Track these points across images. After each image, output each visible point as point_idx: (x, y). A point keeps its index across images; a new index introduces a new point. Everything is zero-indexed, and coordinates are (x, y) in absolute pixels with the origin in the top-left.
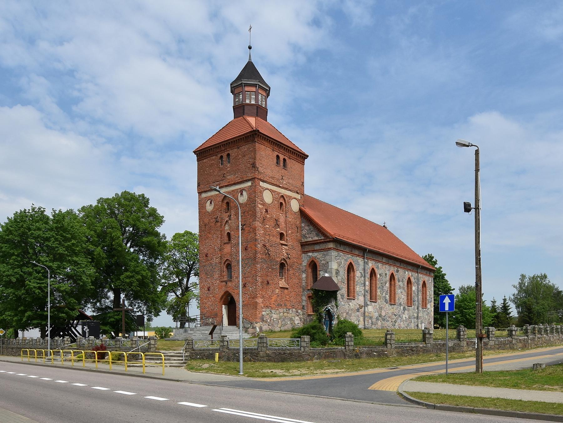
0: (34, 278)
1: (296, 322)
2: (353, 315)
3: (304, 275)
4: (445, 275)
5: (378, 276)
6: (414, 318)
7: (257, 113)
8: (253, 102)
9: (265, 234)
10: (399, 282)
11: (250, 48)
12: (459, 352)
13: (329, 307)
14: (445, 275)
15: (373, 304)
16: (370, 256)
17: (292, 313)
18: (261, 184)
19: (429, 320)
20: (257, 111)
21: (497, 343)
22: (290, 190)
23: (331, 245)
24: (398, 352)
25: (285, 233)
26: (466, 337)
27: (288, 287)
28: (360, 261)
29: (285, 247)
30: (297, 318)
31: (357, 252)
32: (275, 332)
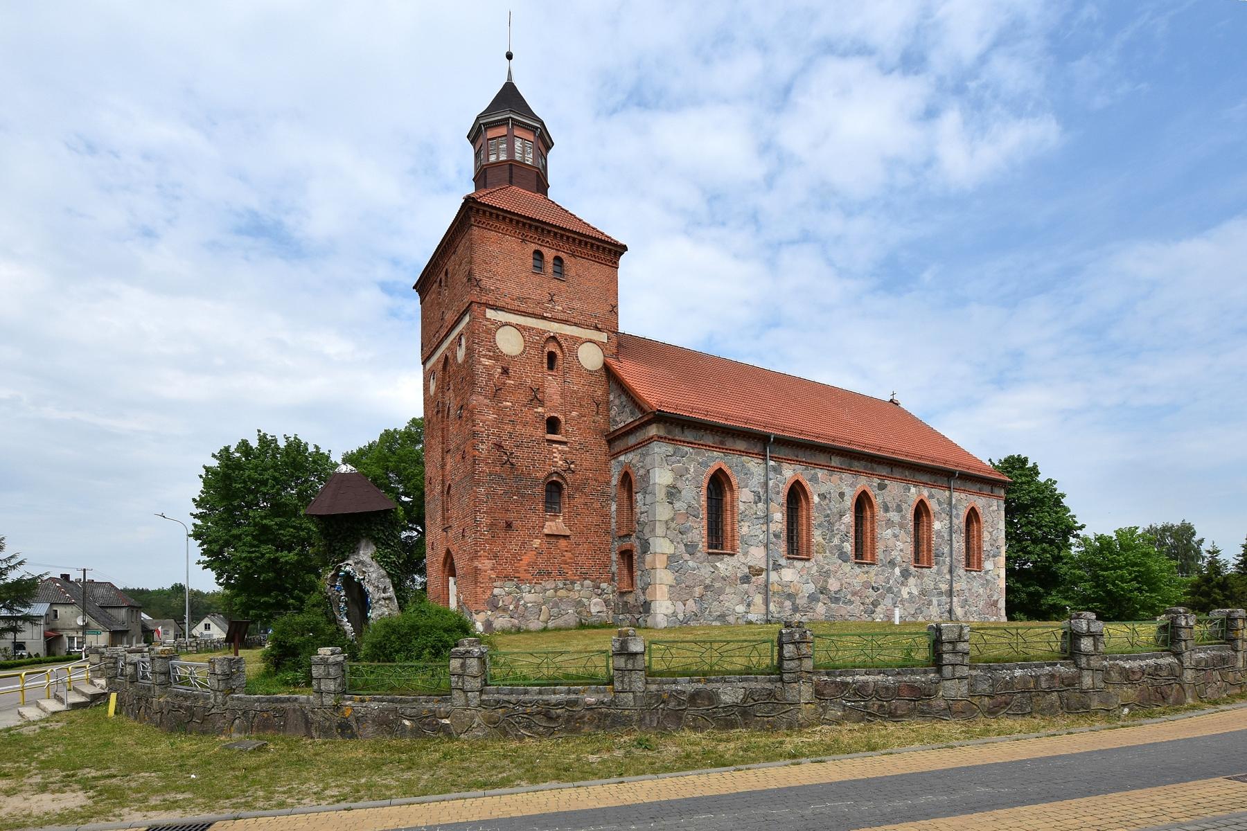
0: (244, 544)
1: (594, 610)
2: (728, 590)
3: (614, 507)
4: (1063, 496)
5: (816, 499)
6: (941, 594)
7: (511, 177)
8: (503, 157)
9: (499, 422)
10: (886, 509)
11: (509, 56)
12: (774, 728)
13: (349, 567)
14: (1063, 496)
15: (798, 564)
16: (783, 452)
17: (581, 590)
18: (490, 314)
19: (990, 596)
20: (511, 173)
21: (984, 687)
22: (576, 324)
23: (653, 430)
24: (492, 722)
25: (561, 418)
26: (808, 664)
27: (568, 533)
28: (754, 466)
29: (560, 447)
30: (596, 600)
31: (741, 445)
32: (528, 631)
